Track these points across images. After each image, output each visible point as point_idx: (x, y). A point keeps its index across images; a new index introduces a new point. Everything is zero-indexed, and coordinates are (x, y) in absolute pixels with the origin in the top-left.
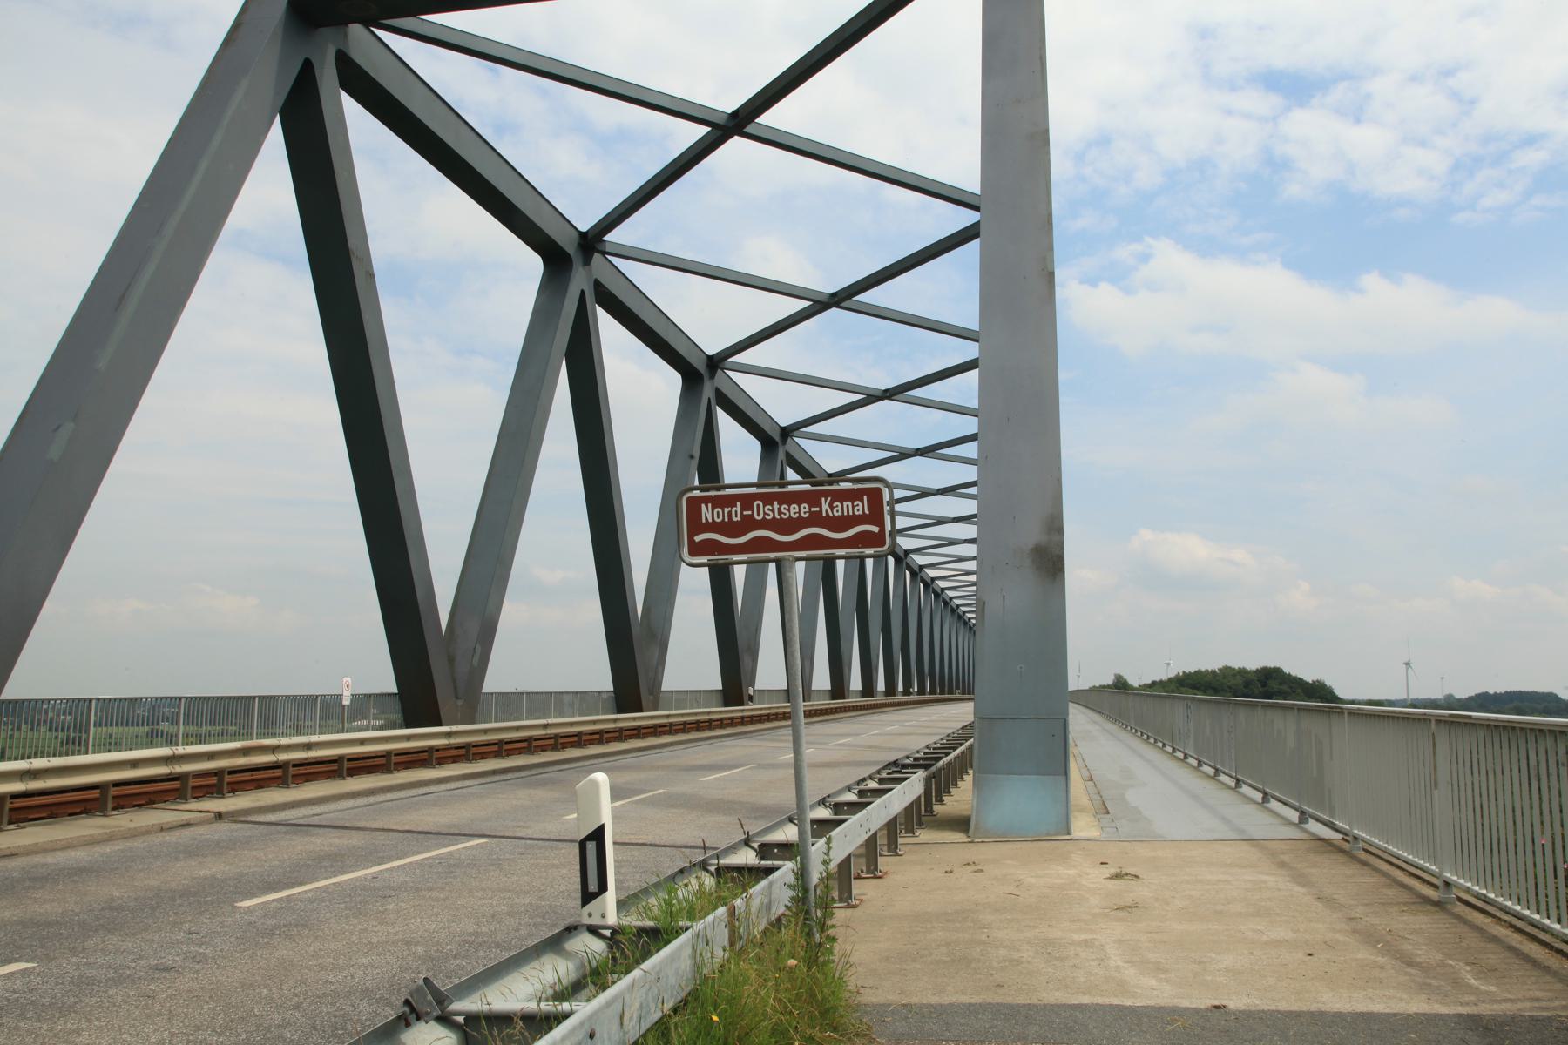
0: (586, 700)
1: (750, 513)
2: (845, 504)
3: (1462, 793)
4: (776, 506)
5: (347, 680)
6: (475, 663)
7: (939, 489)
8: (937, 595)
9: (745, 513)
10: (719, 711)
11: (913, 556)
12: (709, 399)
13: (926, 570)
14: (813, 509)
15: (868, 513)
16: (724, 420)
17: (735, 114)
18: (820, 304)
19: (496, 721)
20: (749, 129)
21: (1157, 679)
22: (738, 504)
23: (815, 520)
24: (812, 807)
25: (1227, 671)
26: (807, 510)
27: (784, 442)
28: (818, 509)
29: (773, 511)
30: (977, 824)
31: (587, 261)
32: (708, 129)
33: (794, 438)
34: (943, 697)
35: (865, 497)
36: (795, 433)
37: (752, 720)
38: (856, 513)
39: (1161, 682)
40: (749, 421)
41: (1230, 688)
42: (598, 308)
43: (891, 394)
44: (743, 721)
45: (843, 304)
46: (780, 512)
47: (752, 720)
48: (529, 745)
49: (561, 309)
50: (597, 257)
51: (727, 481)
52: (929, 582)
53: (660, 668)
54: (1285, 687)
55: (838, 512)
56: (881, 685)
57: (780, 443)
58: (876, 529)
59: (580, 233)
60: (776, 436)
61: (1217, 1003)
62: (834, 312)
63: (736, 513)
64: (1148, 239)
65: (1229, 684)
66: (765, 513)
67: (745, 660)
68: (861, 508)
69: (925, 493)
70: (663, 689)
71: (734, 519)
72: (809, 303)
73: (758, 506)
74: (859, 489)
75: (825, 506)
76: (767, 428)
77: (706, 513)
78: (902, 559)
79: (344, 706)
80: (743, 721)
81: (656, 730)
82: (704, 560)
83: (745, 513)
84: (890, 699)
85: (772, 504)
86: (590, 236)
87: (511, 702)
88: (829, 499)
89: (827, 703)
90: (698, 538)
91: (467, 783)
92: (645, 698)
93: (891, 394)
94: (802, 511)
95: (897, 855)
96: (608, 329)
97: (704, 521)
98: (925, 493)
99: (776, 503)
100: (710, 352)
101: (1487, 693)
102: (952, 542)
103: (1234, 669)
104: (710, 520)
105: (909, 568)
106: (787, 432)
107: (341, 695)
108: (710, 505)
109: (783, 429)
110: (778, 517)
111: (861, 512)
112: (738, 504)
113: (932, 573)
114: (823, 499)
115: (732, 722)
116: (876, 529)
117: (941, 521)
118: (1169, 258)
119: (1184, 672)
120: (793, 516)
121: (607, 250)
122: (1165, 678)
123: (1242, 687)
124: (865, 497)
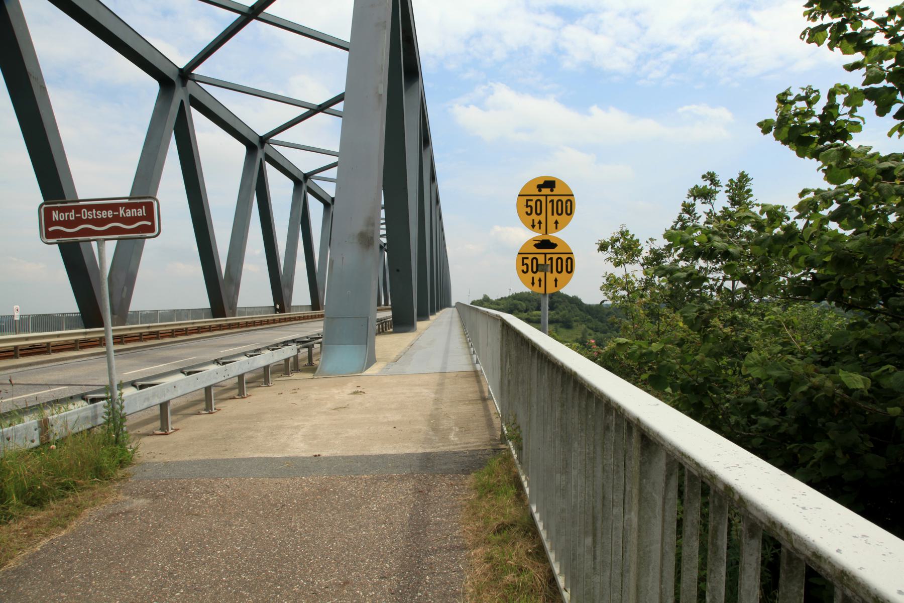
0: (196, 313)
1: (79, 215)
2: (133, 210)
4: (94, 211)
5: (16, 307)
6: (124, 296)
9: (77, 215)
12: (261, 159)
14: (115, 213)
15: (145, 214)
16: (270, 169)
17: (253, 7)
18: (314, 110)
19: (141, 324)
20: (260, 16)
21: (503, 297)
22: (73, 211)
23: (116, 219)
26: (112, 213)
27: (306, 181)
28: (117, 213)
29: (92, 214)
30: (321, 368)
31: (184, 84)
32: (239, 15)
35: (144, 207)
36: (311, 177)
37: (290, 319)
38: (139, 215)
39: (505, 297)
41: (536, 300)
42: (192, 108)
44: (285, 320)
45: (325, 111)
46: (96, 215)
47: (290, 319)
49: (169, 109)
50: (190, 82)
51: (80, 198)
53: (236, 296)
54: (560, 299)
56: (383, 303)
58: (149, 223)
60: (301, 178)
61: (315, 454)
63: (72, 215)
64: (491, 84)
66: (88, 216)
67: (285, 292)
68: (141, 212)
70: (292, 305)
71: (71, 219)
72: (308, 110)
73: (84, 212)
74: (140, 202)
75: (122, 212)
76: (296, 174)
79: (16, 321)
80: (285, 320)
82: (55, 240)
83: (77, 215)
85: (92, 211)
86: (184, 71)
87: (149, 316)
88: (124, 208)
90: (51, 229)
91: (92, 358)
92: (227, 311)
94: (109, 214)
95: (269, 386)
96: (197, 118)
97: (54, 220)
99: (94, 210)
104: (57, 219)
106: (307, 176)
107: (14, 316)
108: (57, 212)
109: (305, 175)
110: (95, 217)
111: (141, 215)
112: (73, 211)
114: (120, 208)
116: (149, 223)
118: (503, 94)
120: (104, 217)
121: (195, 79)
122: (507, 296)
124: (144, 207)
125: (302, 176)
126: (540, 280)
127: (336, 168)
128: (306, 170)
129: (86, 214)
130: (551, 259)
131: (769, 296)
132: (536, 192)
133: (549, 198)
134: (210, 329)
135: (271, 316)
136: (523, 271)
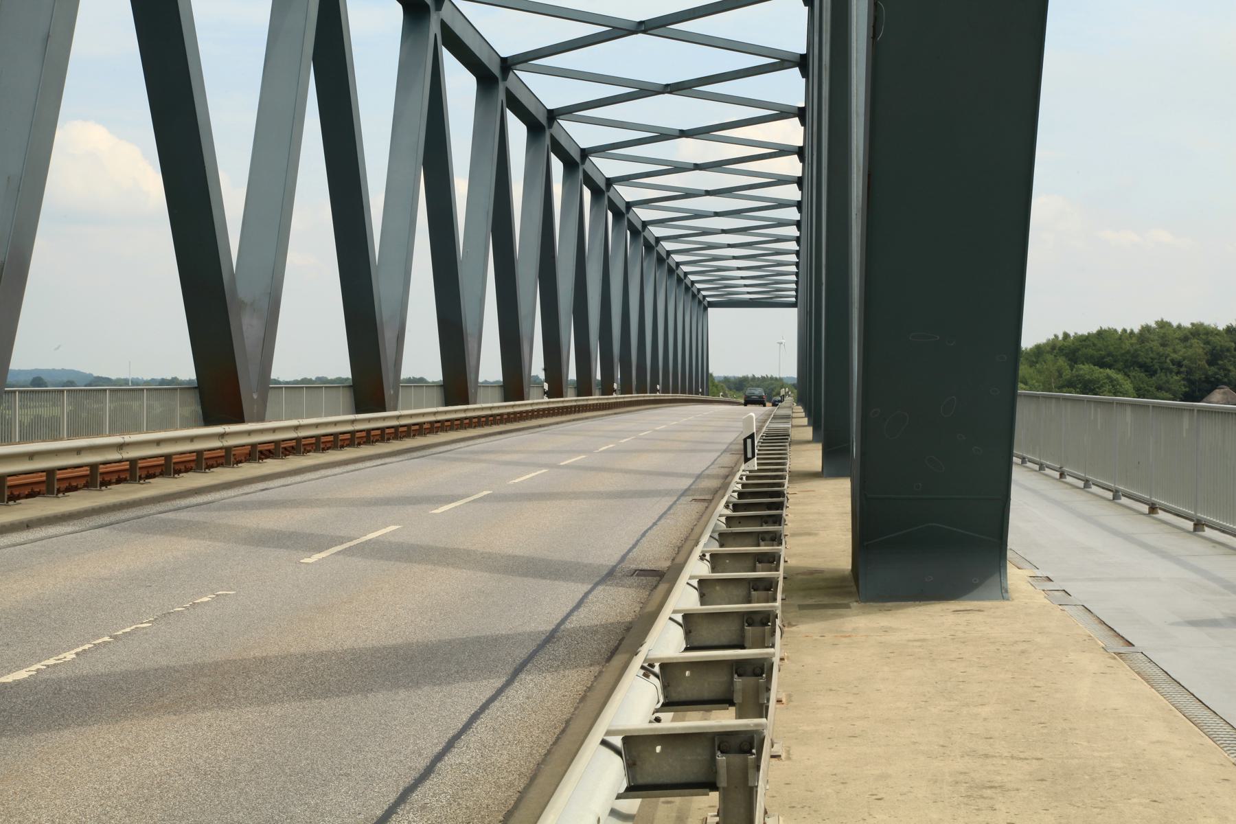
7: (667, 85)
8: (636, 233)
10: (344, 419)
12: (436, 35)
13: (594, 159)
24: (774, 396)
25: (1163, 333)
33: (515, 71)
34: (641, 397)
36: (518, 66)
41: (1179, 364)
42: (507, 110)
43: (644, 27)
44: (384, 435)
48: (95, 478)
52: (623, 209)
57: (546, 128)
60: (495, 69)
65: (1174, 356)
67: (247, 328)
69: (645, 91)
78: (640, 231)
80: (384, 435)
81: (257, 453)
84: (556, 402)
89: (435, 410)
93: (644, 27)
98: (645, 91)
102: (689, 194)
105: (589, 181)
106: (507, 65)
113: (644, 214)
115: (369, 438)
117: (664, 135)
119: (1066, 336)
123: (1203, 363)
125: (625, 205)
128: (506, 50)
134: (201, 462)
135: (344, 419)
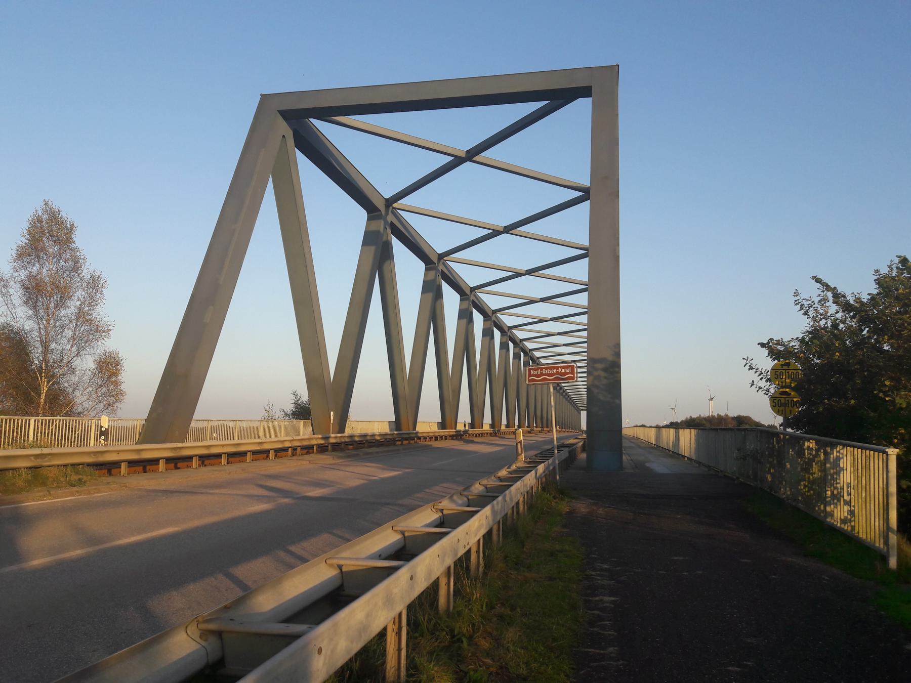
3: (868, 505)
11: (534, 352)
40: (456, 285)
55: (563, 371)
58: (572, 376)
59: (385, 199)
62: (505, 236)
63: (539, 372)
68: (569, 370)
75: (560, 370)
77: (532, 372)
98: (542, 321)
100: (439, 252)
101: (740, 415)
103: (763, 426)
116: (572, 376)
126: (782, 411)
127: (587, 259)
129: (545, 371)
130: (788, 400)
131: (770, 480)
132: (780, 368)
133: (787, 371)
136: (773, 406)
